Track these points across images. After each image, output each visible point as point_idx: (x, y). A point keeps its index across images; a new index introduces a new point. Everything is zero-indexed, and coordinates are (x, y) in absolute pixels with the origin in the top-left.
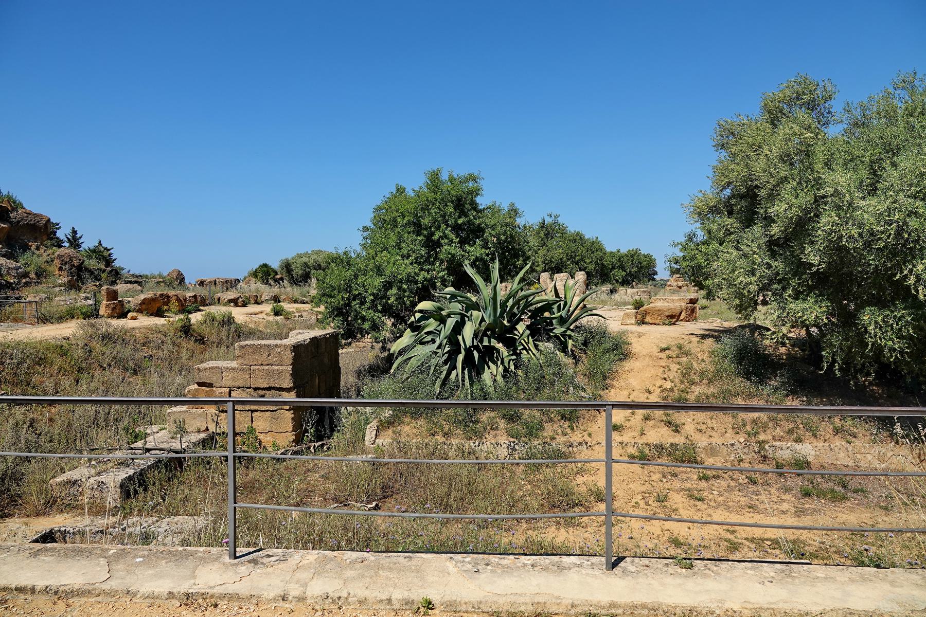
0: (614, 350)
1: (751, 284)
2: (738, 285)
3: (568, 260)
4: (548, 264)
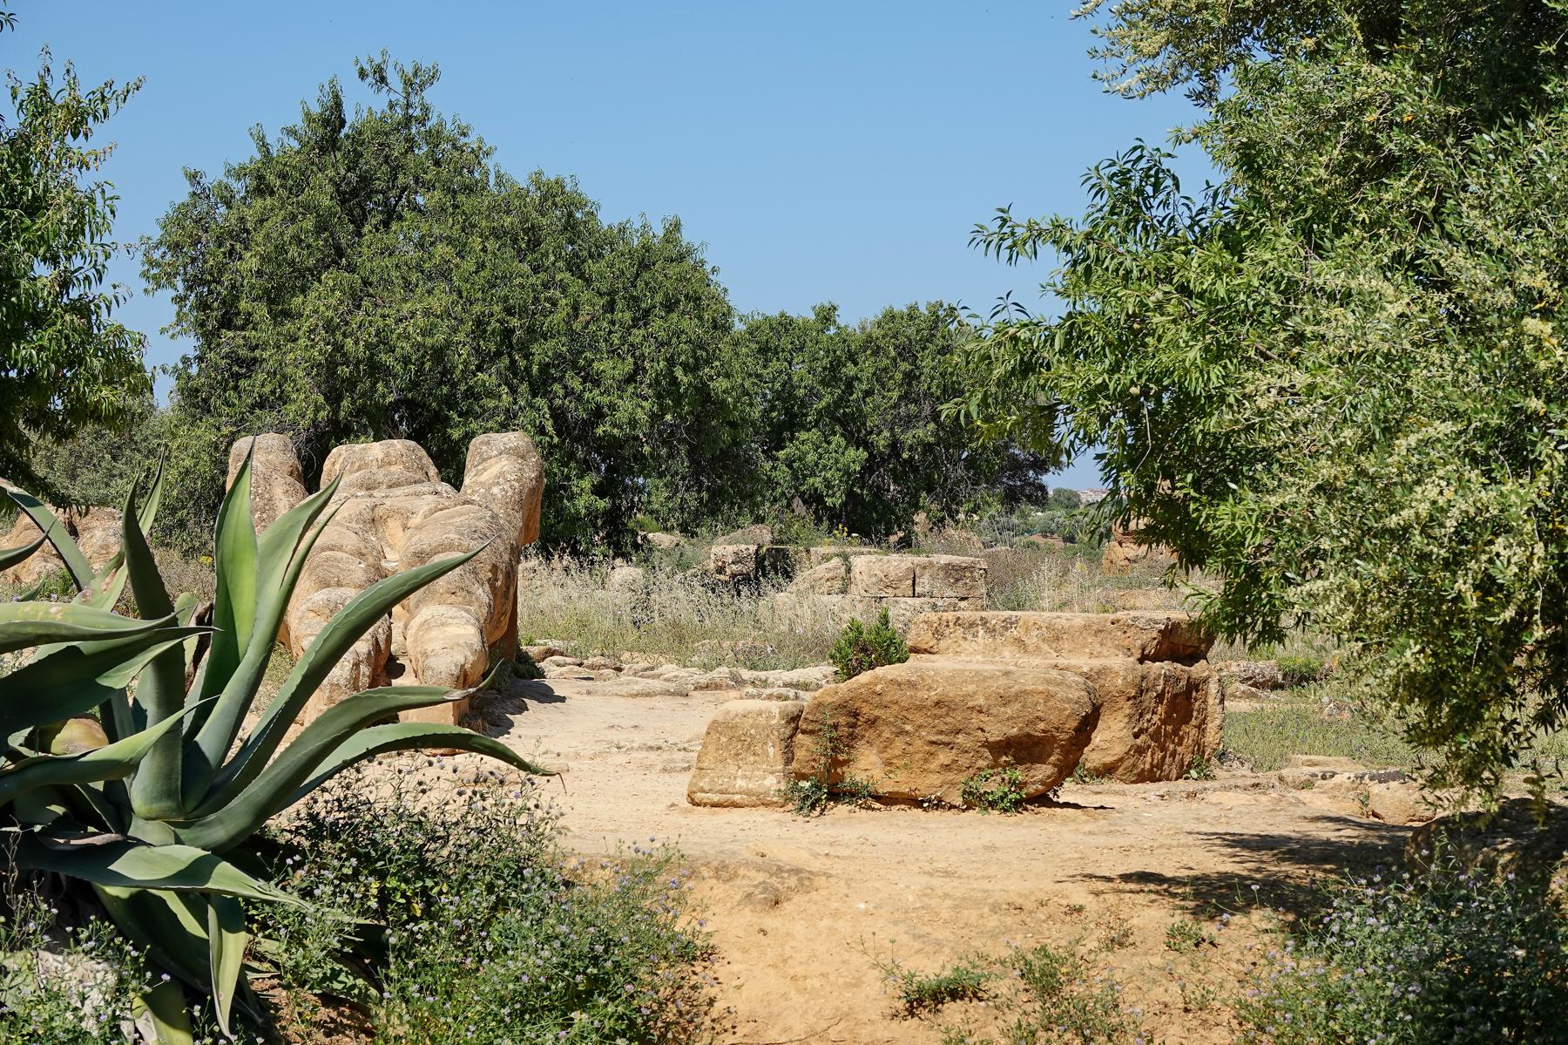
0: (581, 1000)
1: (1501, 527)
2: (1417, 540)
3: (485, 360)
4: (352, 383)
